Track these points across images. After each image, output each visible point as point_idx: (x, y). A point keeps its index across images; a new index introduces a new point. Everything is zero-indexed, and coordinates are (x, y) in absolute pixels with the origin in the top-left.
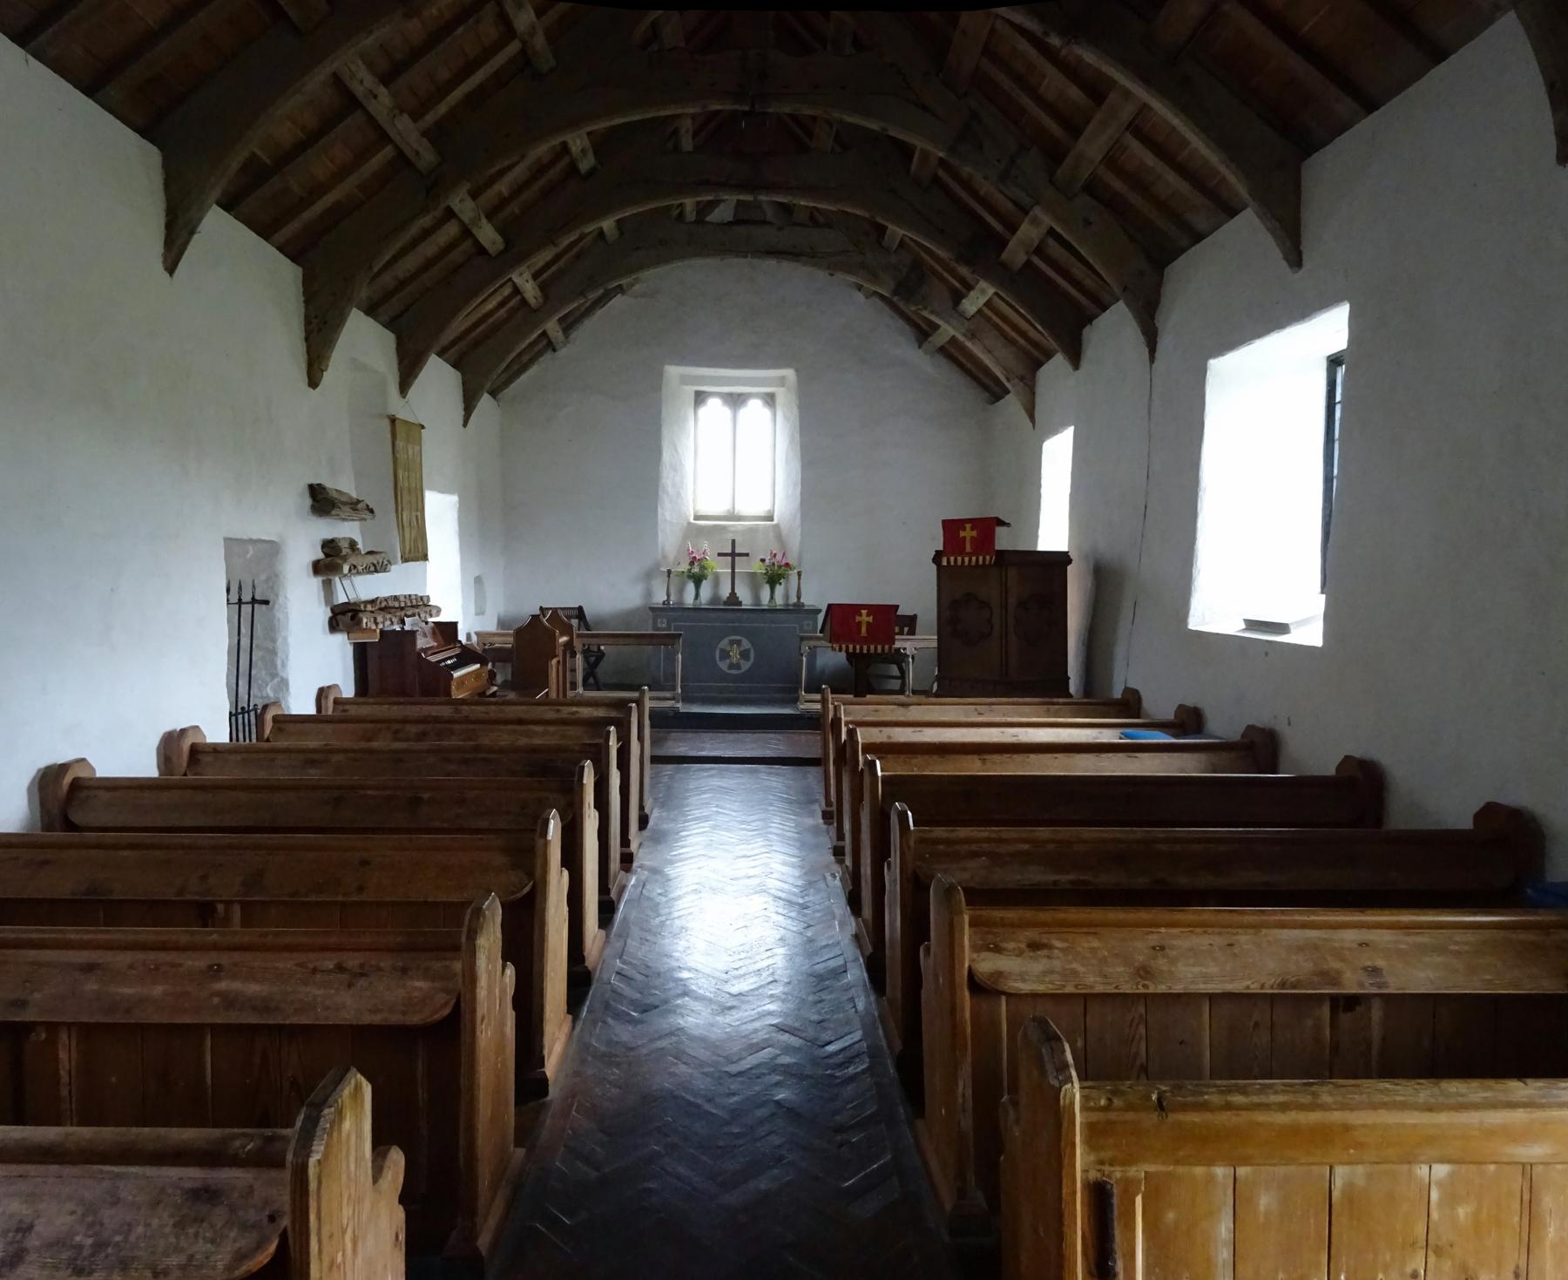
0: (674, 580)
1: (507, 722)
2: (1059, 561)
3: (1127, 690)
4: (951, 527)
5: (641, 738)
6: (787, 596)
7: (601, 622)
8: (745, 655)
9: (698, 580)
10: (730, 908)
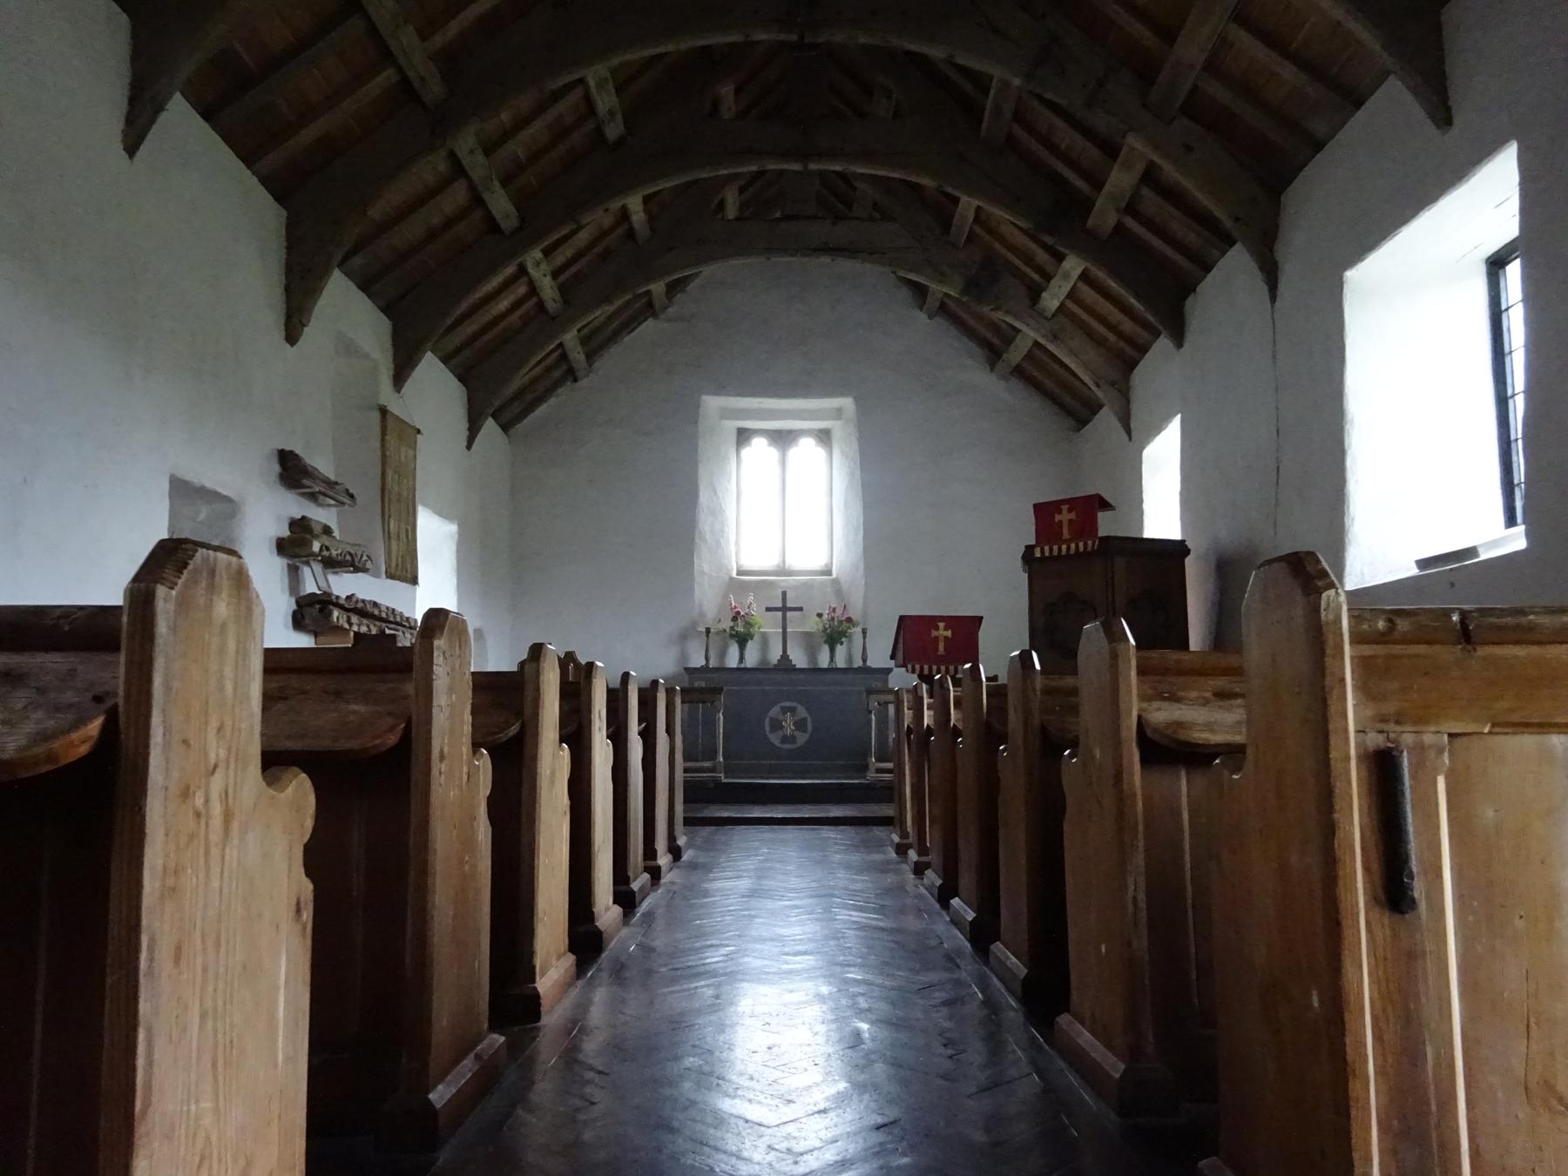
0: (715, 643)
2: (1173, 552)
5: (670, 730)
6: (850, 659)
8: (800, 725)
9: (742, 640)
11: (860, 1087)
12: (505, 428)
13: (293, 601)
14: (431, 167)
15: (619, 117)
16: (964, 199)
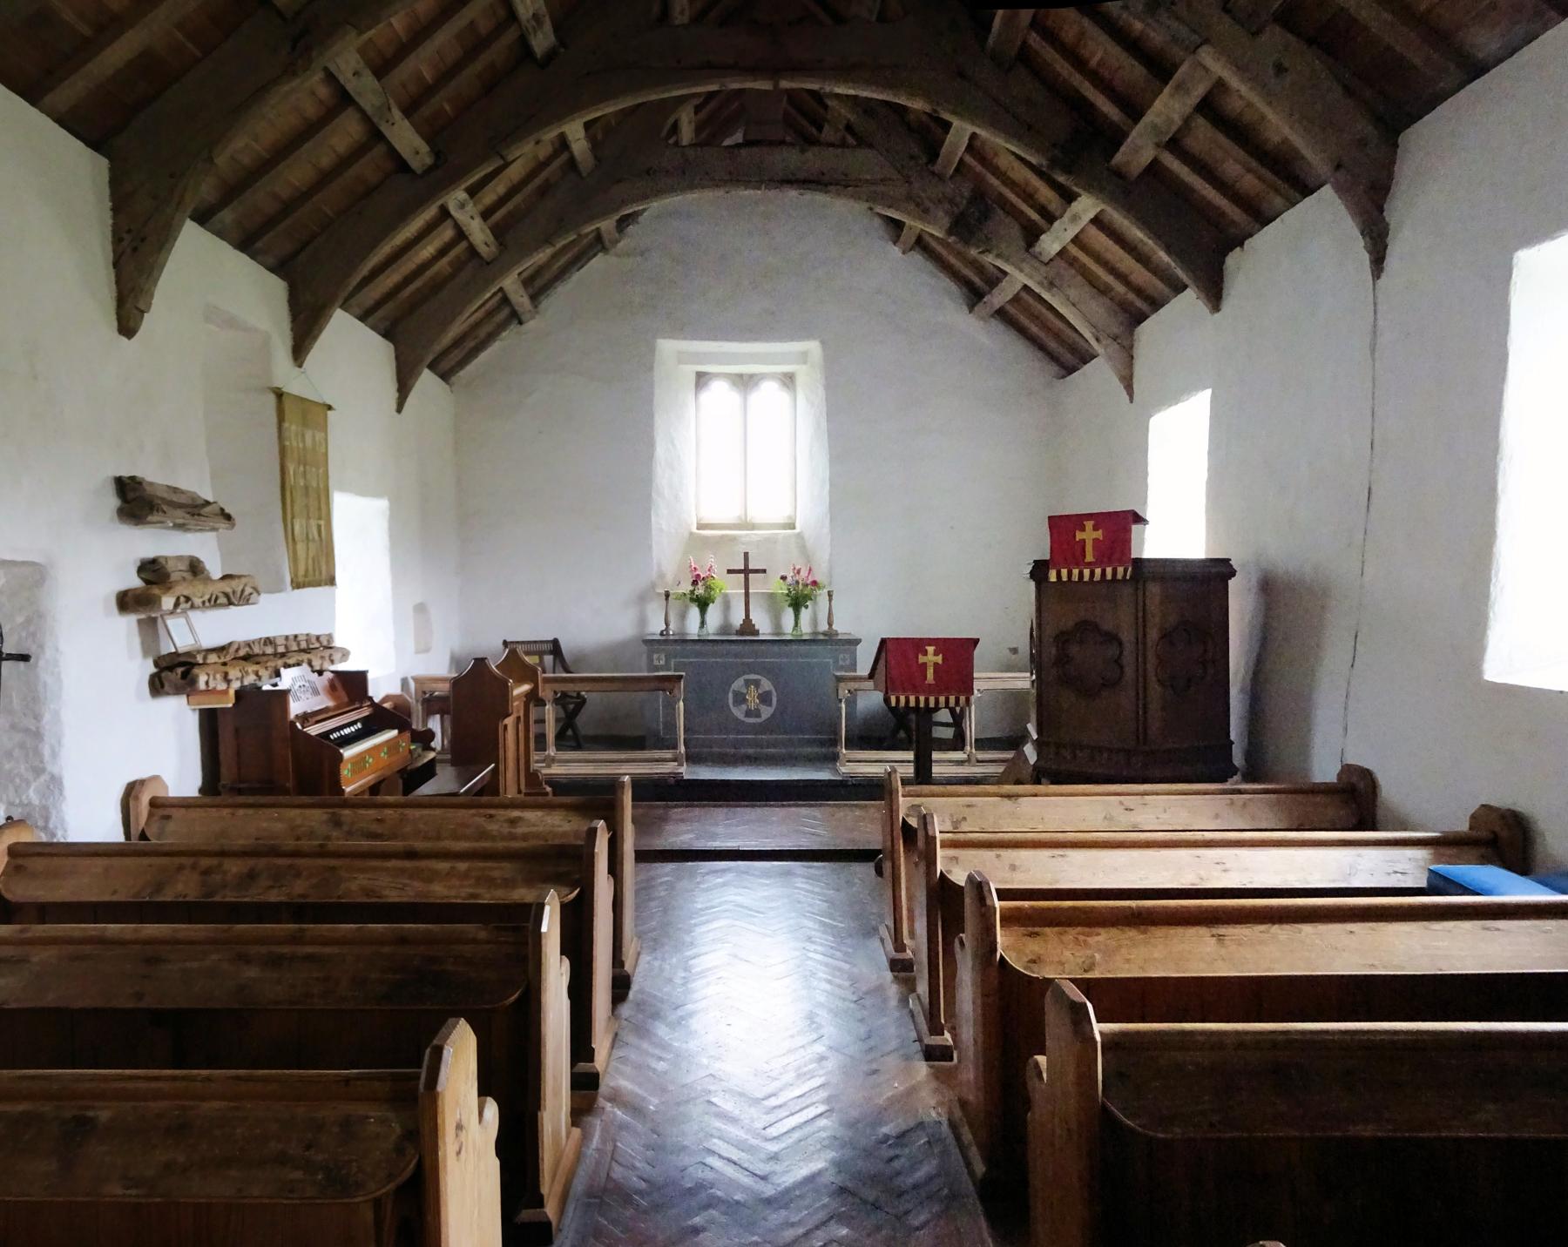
1: (386, 855)
2: (1216, 573)
3: (1347, 769)
4: (1063, 527)
6: (815, 622)
7: (582, 659)
8: (765, 698)
9: (703, 604)
12: (445, 376)
13: (150, 663)
14: (301, 95)
15: (548, 26)
16: (956, 122)
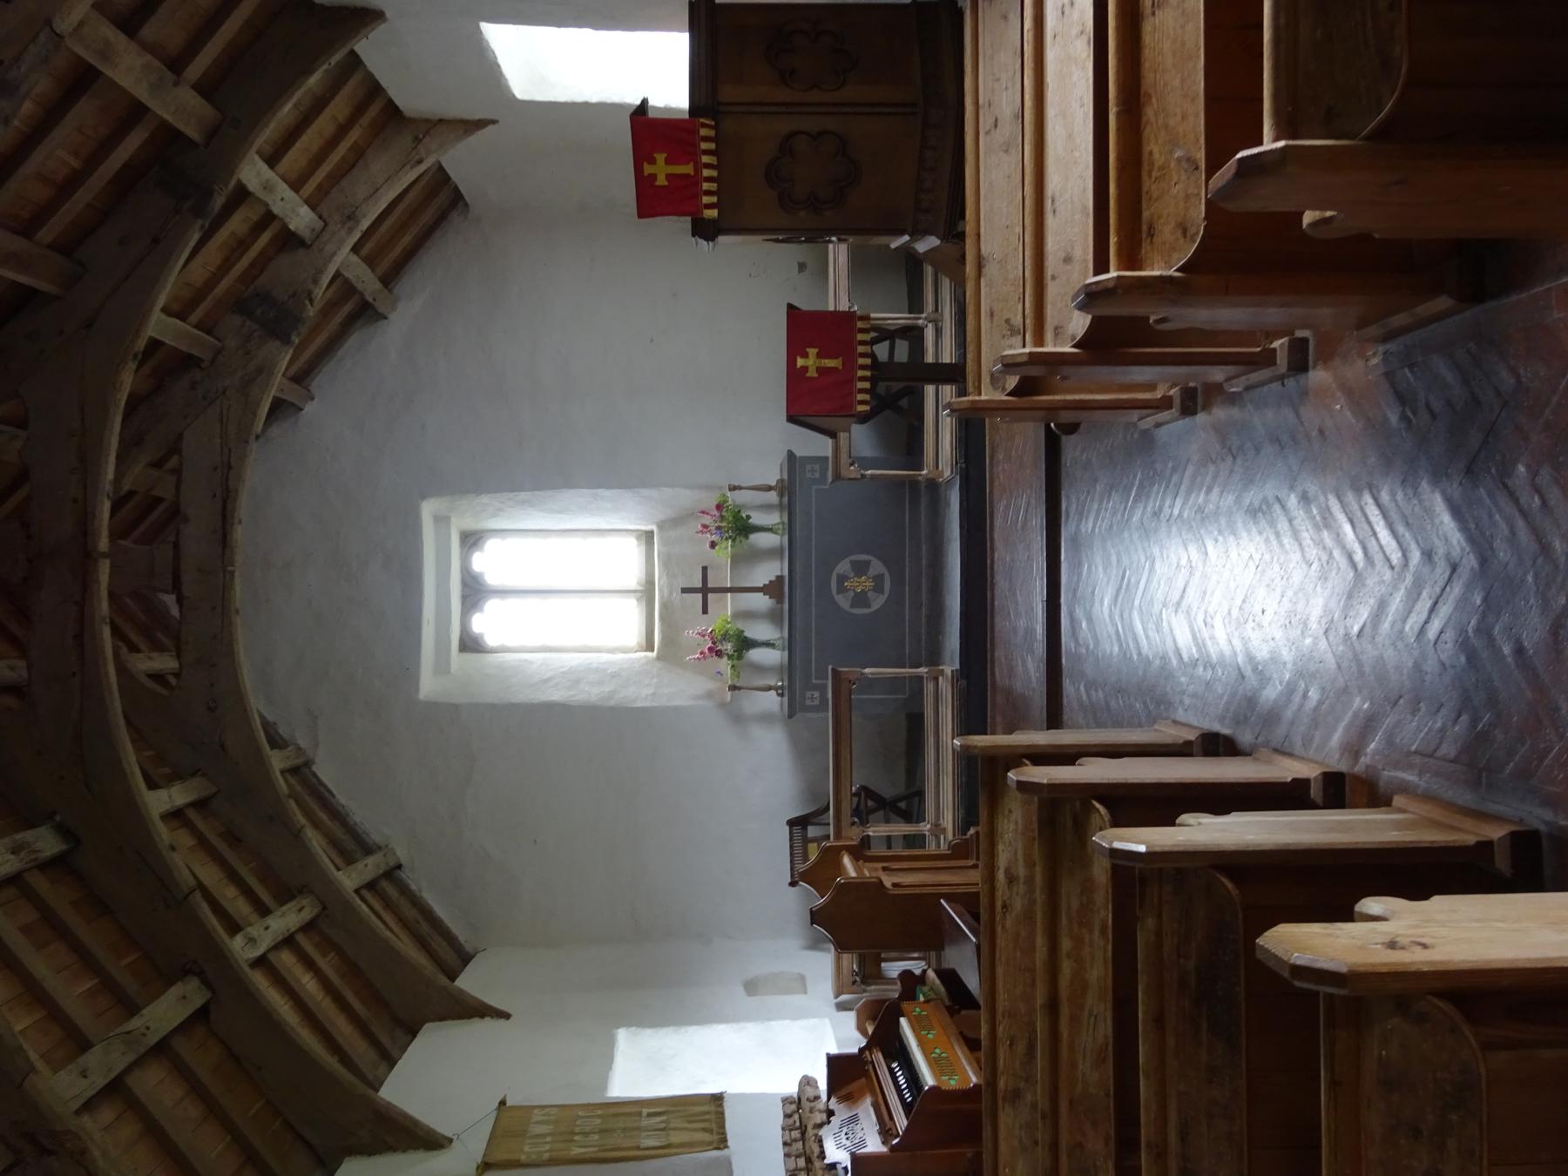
6: (767, 507)
7: (812, 790)
8: (860, 569)
9: (745, 644)
10: (1243, 589)
11: (1409, 481)
12: (466, 959)
16: (151, 331)
